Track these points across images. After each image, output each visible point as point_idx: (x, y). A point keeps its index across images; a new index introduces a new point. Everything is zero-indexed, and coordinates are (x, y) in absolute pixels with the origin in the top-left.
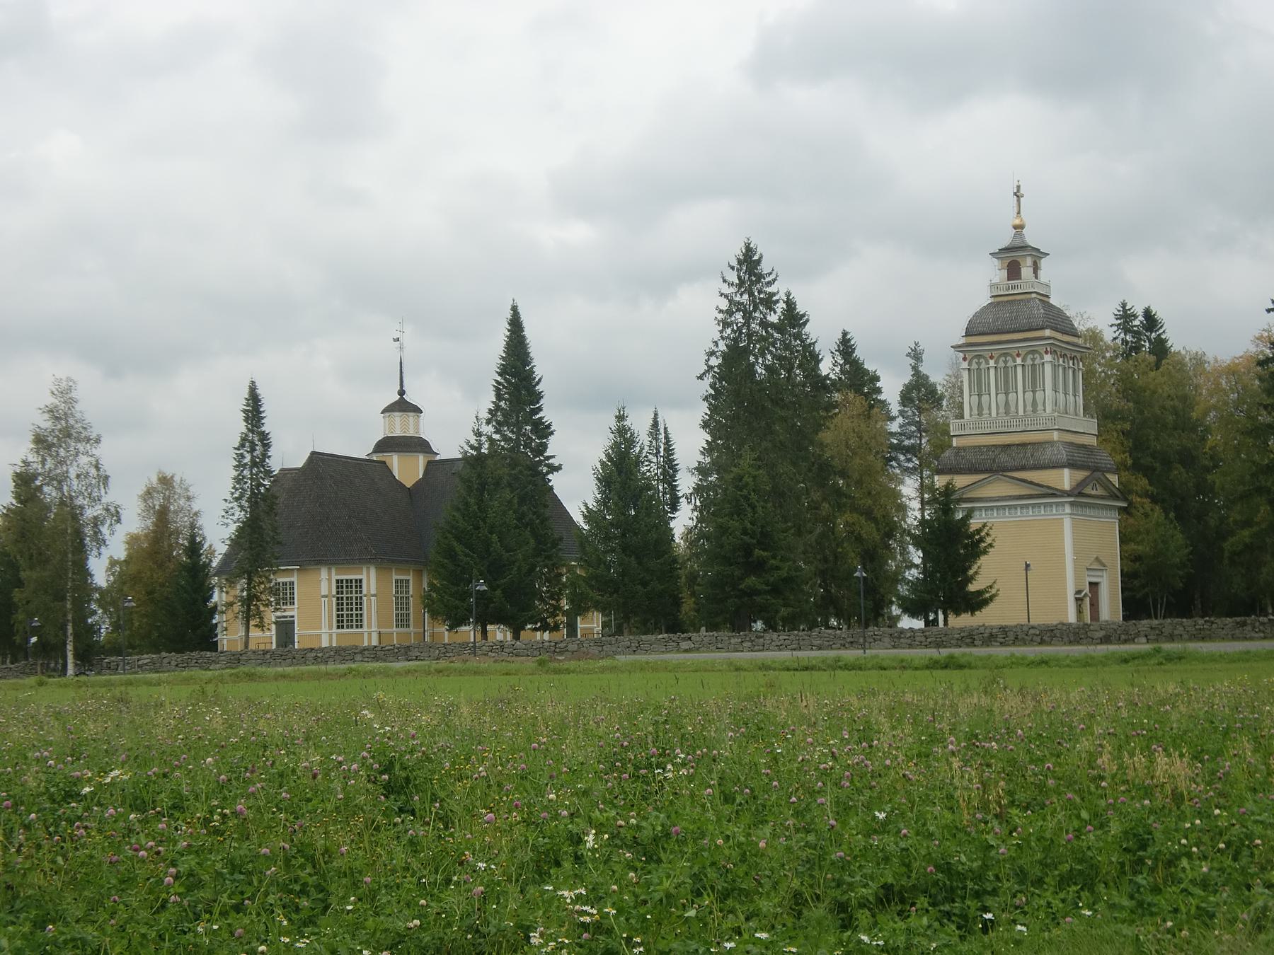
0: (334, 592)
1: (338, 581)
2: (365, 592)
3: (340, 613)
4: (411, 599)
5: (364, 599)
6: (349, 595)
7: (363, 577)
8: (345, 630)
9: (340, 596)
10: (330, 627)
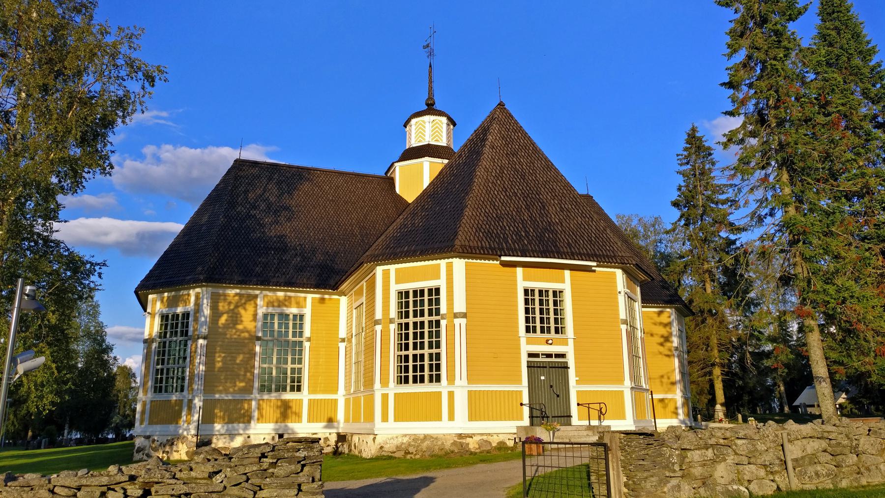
4: (307, 345)
5: (443, 323)
8: (411, 388)
10: (385, 383)
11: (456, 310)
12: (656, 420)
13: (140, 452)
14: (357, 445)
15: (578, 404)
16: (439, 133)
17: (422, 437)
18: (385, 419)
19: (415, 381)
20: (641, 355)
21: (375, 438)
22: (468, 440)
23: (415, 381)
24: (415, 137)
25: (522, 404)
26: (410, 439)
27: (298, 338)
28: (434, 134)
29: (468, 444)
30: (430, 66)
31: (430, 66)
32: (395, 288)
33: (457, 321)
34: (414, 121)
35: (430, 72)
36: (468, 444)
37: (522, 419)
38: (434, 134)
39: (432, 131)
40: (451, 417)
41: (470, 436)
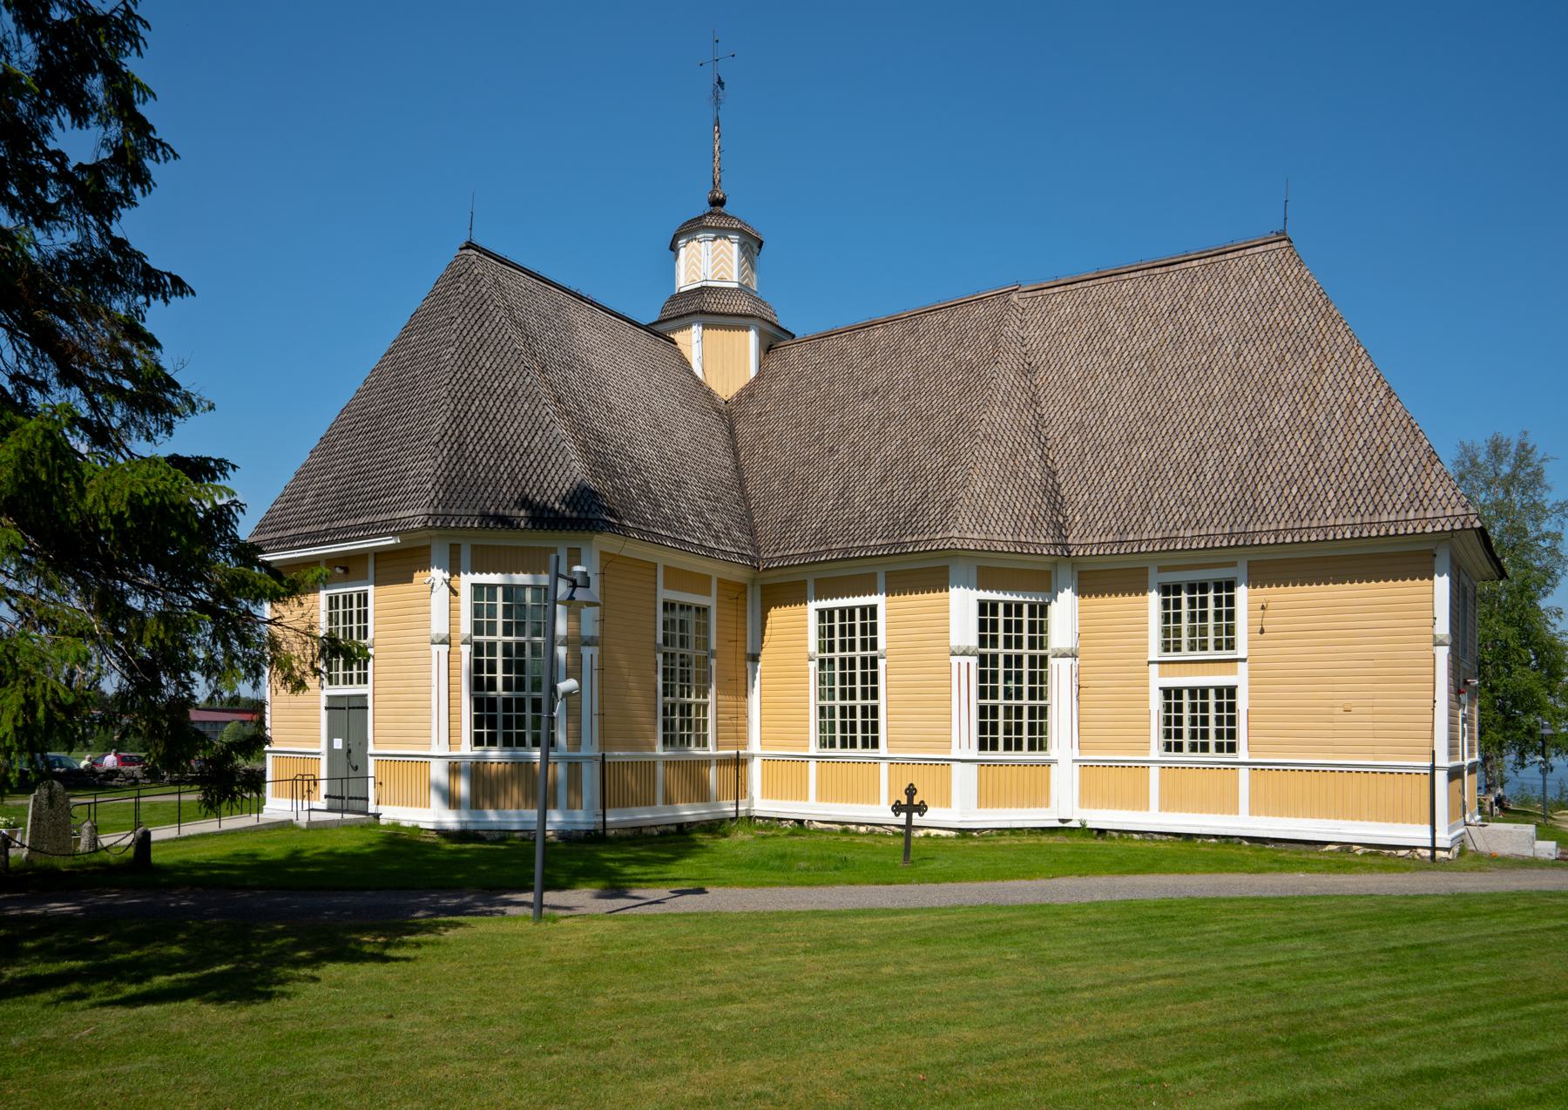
3: (988, 702)
6: (1013, 651)
12: (608, 811)
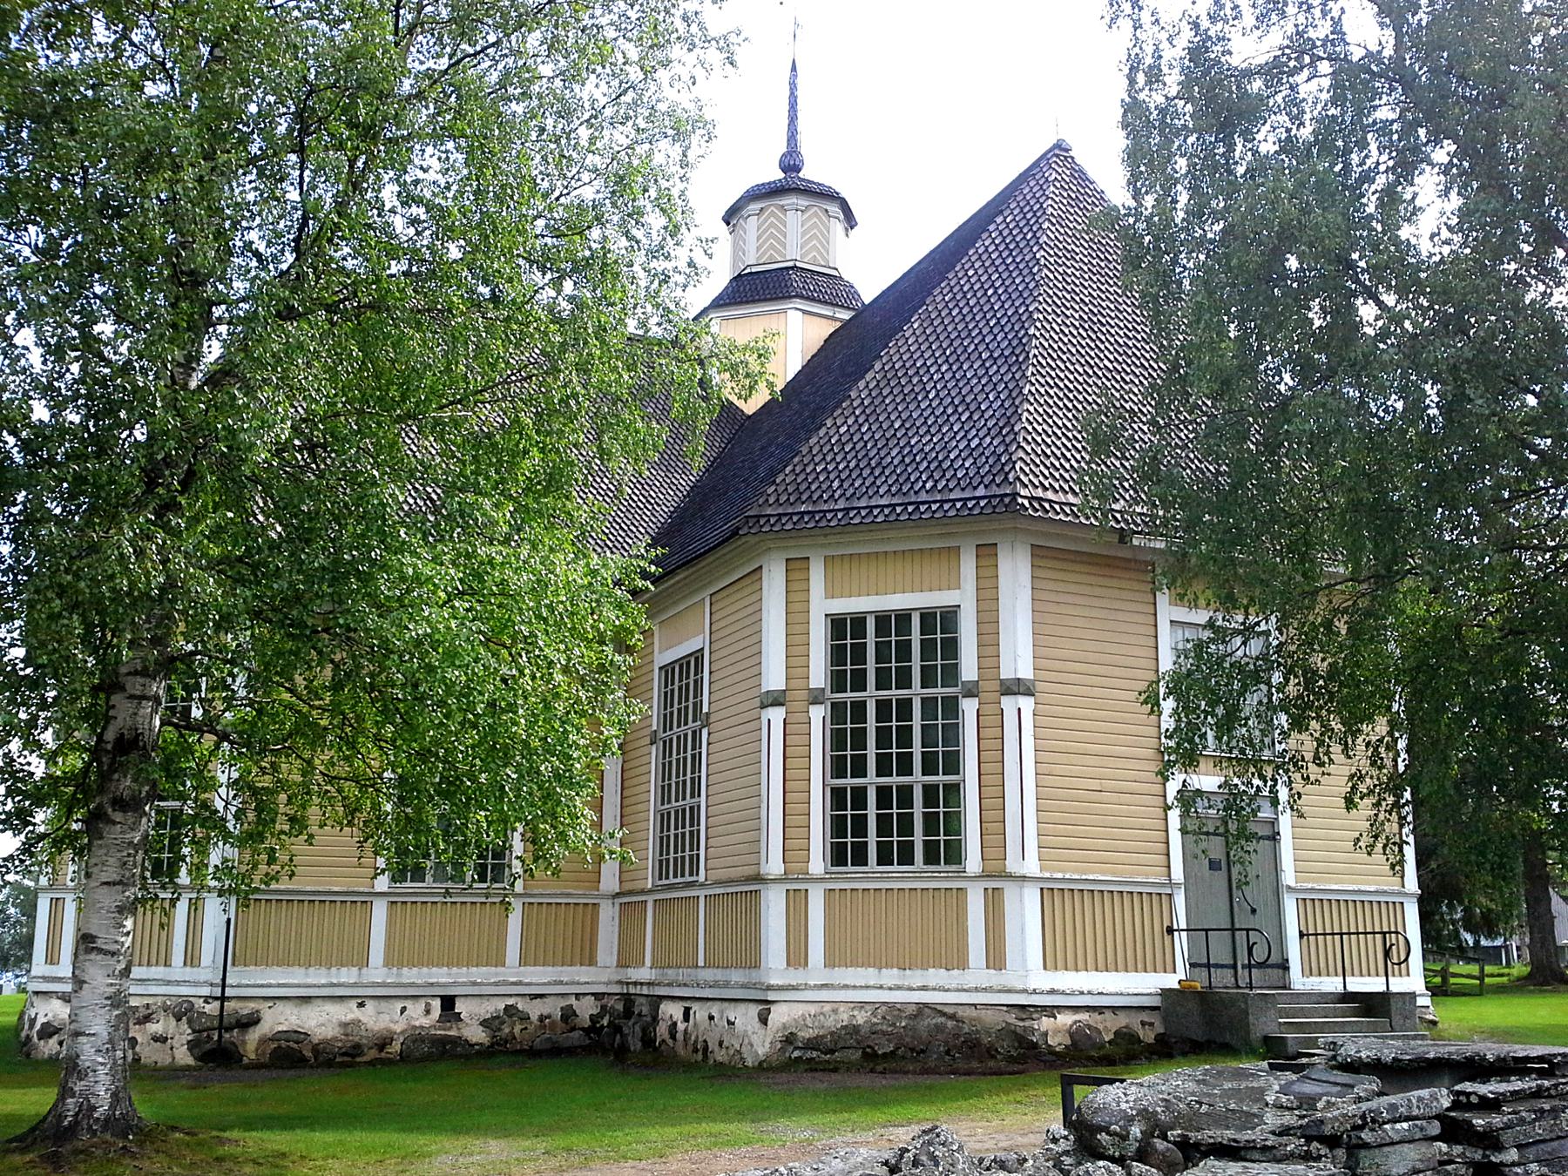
0: (819, 675)
1: (837, 625)
2: (969, 669)
5: (969, 707)
6: (894, 693)
7: (963, 597)
9: (849, 696)
11: (1006, 673)
13: (50, 1036)
14: (681, 1026)
15: (1301, 935)
16: (821, 243)
17: (911, 1009)
18: (797, 955)
19: (884, 859)
20: (774, 865)
21: (769, 1010)
22: (1045, 1023)
23: (884, 859)
24: (758, 249)
25: (1170, 931)
26: (874, 1014)
27: (919, 663)
28: (806, 242)
29: (1046, 1034)
30: (794, 68)
31: (794, 68)
32: (822, 605)
33: (1008, 703)
34: (755, 207)
35: (793, 86)
36: (1046, 1034)
37: (1308, 971)
38: (806, 242)
39: (803, 234)
40: (996, 959)
41: (1051, 1011)
